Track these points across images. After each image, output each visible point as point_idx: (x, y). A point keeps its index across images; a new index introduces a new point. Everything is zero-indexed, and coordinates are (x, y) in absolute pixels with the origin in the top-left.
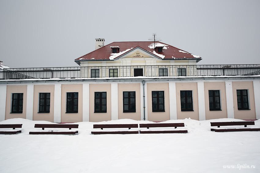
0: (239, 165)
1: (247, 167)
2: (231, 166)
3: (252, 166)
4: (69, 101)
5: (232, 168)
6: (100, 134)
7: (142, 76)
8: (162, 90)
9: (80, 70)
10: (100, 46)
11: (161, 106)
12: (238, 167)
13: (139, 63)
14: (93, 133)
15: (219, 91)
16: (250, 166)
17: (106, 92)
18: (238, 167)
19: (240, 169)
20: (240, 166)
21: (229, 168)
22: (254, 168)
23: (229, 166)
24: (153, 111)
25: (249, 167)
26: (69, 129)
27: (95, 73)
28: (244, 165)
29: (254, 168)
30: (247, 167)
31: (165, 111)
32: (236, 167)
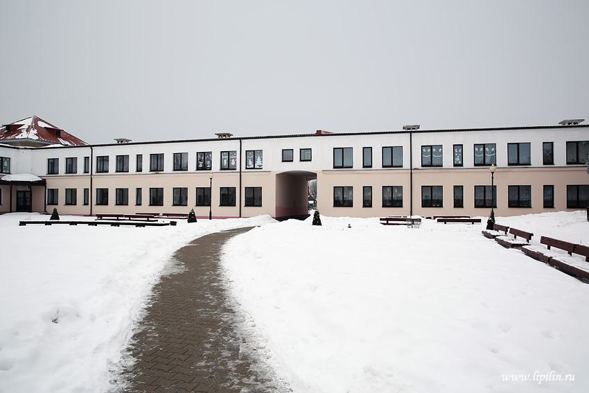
1: (555, 377)
5: (513, 379)
6: (572, 268)
7: (246, 206)
8: (248, 208)
11: (494, 204)
12: (536, 377)
15: (402, 207)
16: (563, 376)
17: (364, 187)
20: (541, 376)
21: (507, 379)
22: (573, 379)
24: (422, 206)
26: (189, 222)
27: (411, 169)
28: (549, 374)
29: (573, 379)
30: (555, 377)
31: (530, 207)
32: (531, 377)
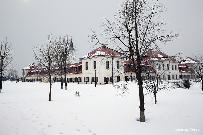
0: (192, 129)
1: (193, 130)
2: (181, 129)
3: (197, 129)
4: (133, 65)
5: (178, 131)
9: (73, 58)
10: (107, 62)
12: (186, 130)
13: (46, 77)
14: (66, 89)
18: (186, 130)
19: (187, 132)
20: (188, 129)
22: (199, 131)
23: (183, 129)
25: (195, 130)
28: (191, 129)
29: (199, 131)
30: (193, 130)
32: (185, 130)
